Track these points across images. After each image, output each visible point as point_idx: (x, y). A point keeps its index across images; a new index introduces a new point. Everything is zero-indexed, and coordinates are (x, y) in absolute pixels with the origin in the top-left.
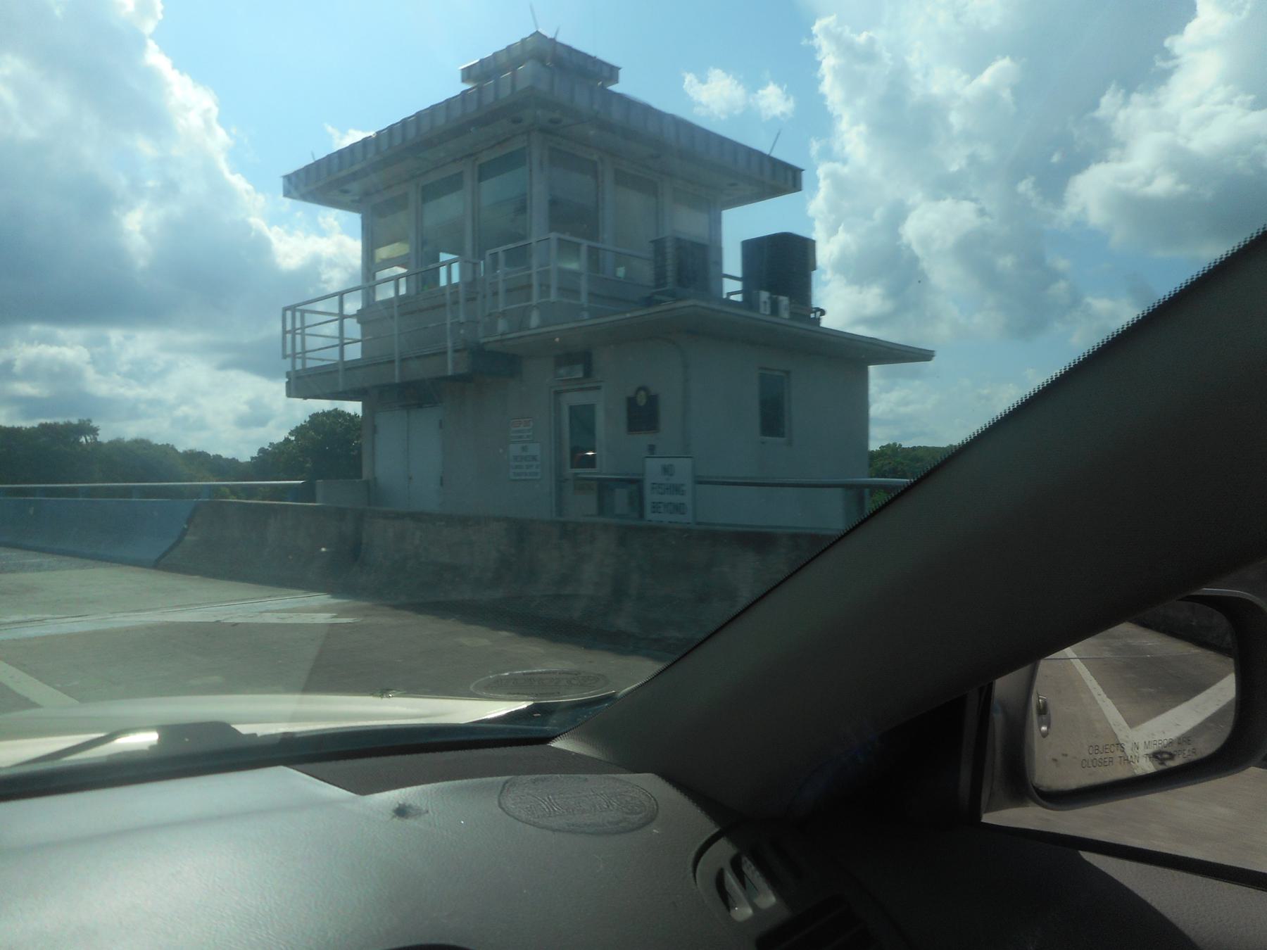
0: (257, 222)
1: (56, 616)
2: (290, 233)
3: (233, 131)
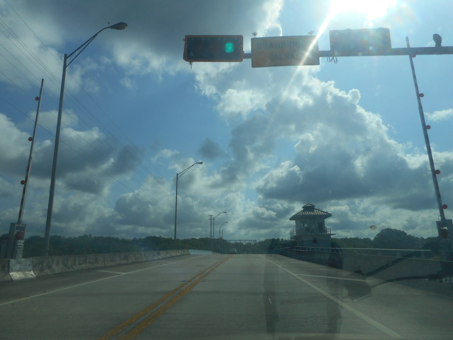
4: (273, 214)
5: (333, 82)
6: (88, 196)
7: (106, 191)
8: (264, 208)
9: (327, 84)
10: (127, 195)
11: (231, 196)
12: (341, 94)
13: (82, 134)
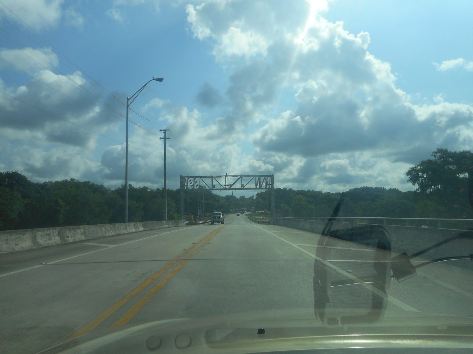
0: (407, 104)
1: (204, 222)
2: (421, 106)
3: (396, 74)
4: (271, 167)
5: (342, 23)
6: (72, 150)
7: (92, 143)
8: (261, 162)
9: (335, 25)
10: (114, 147)
11: (227, 148)
12: (351, 37)
13: (63, 78)
